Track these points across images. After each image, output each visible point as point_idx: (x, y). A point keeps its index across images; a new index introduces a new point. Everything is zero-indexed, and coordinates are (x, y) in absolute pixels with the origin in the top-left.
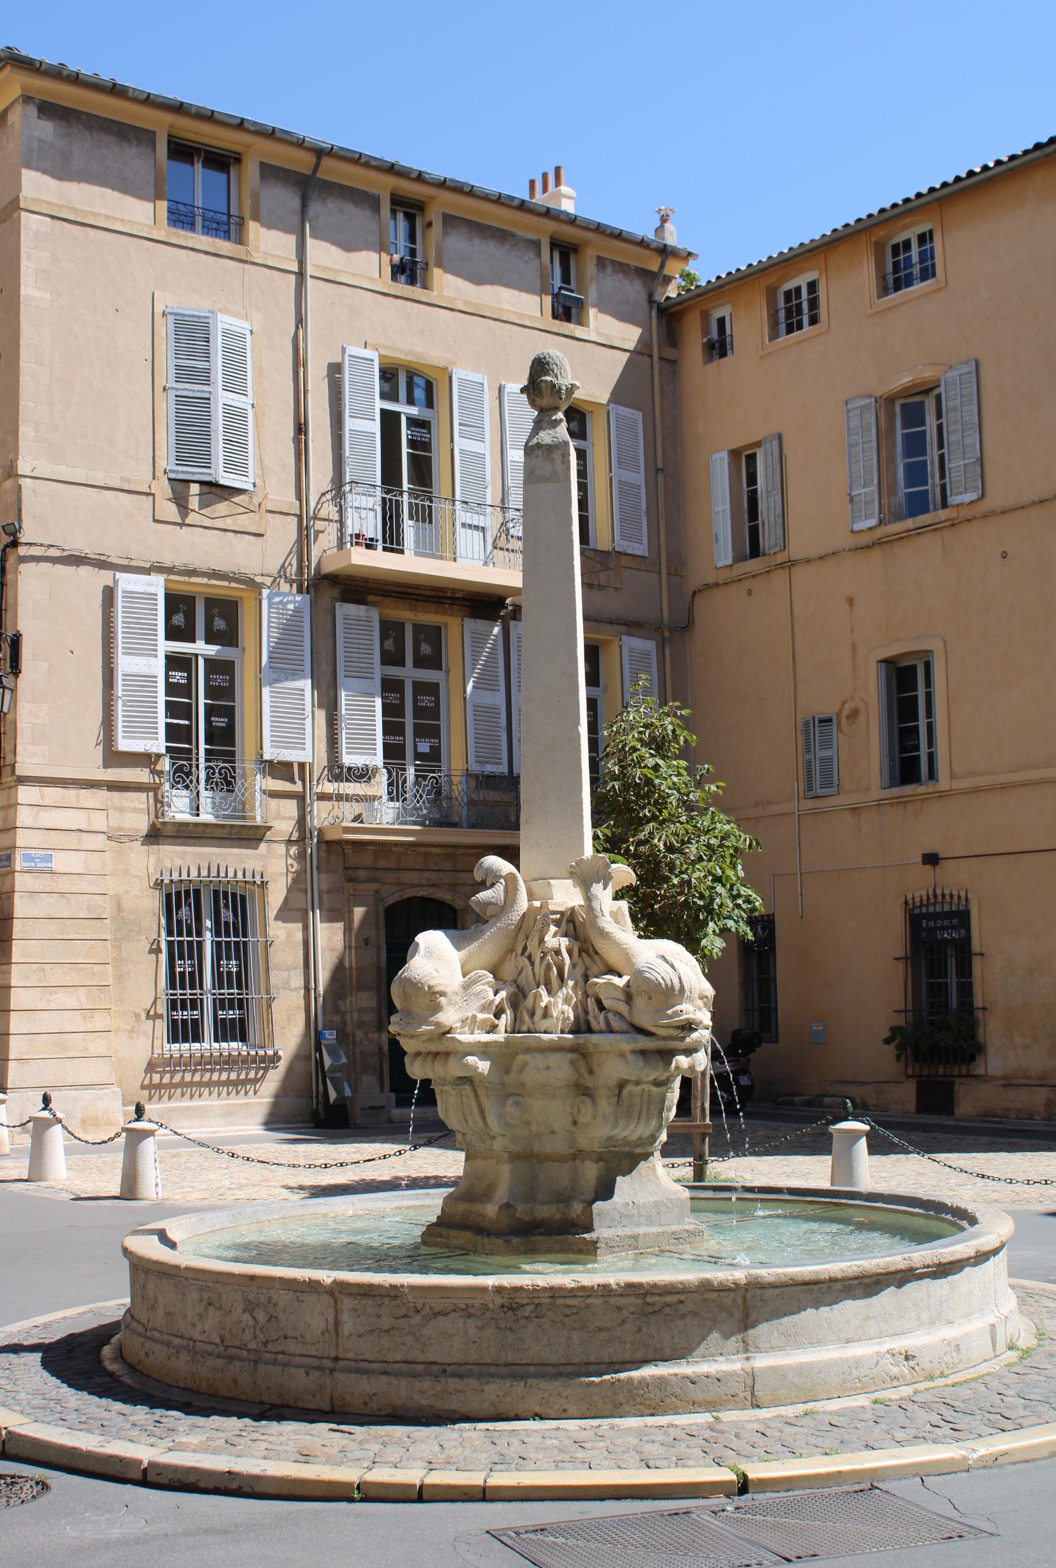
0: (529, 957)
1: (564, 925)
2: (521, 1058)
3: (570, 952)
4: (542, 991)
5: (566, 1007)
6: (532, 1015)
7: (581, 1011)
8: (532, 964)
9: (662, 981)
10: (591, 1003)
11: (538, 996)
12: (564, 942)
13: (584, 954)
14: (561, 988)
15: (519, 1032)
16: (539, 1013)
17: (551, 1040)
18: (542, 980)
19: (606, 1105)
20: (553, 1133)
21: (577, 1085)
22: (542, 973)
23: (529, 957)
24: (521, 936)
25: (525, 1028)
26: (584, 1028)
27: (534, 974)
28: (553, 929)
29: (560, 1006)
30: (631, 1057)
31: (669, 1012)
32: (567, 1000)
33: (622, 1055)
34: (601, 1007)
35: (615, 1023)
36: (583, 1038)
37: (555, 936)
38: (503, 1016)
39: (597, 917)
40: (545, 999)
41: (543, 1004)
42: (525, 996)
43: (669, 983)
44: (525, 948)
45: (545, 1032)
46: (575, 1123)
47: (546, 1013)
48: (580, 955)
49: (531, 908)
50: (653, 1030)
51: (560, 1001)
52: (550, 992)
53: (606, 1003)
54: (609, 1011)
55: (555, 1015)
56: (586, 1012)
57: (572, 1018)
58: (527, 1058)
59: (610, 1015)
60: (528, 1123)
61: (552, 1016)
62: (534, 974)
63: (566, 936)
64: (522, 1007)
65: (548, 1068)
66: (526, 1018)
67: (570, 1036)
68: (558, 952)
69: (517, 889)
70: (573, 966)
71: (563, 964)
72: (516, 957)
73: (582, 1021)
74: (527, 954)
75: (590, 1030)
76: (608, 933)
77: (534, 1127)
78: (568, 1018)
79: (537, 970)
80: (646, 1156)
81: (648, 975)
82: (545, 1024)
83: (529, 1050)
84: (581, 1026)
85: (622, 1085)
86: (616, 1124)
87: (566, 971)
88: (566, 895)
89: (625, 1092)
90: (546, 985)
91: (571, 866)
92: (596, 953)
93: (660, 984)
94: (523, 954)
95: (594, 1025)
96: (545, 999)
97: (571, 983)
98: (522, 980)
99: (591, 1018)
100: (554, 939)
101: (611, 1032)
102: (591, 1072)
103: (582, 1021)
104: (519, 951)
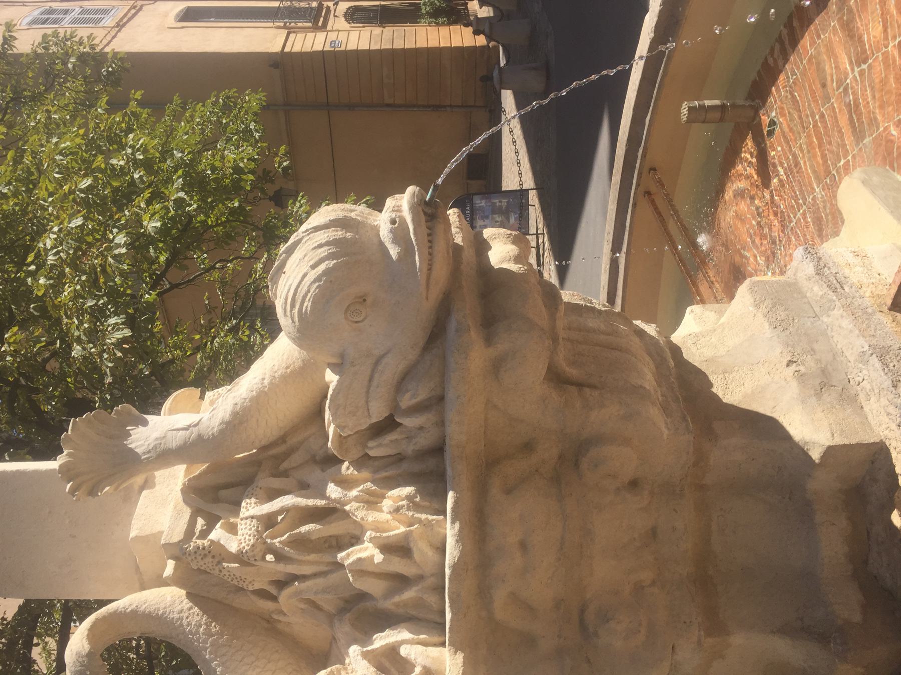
0: (282, 584)
1: (216, 509)
2: (501, 609)
3: (272, 495)
4: (349, 556)
5: (387, 504)
6: (401, 581)
7: (391, 470)
8: (295, 578)
9: (322, 267)
10: (378, 449)
11: (362, 569)
12: (251, 508)
13: (285, 465)
14: (346, 515)
15: (443, 613)
16: (399, 566)
17: (461, 538)
18: (327, 558)
19: (605, 415)
20: (653, 533)
21: (556, 480)
22: (312, 557)
23: (282, 584)
24: (239, 601)
25: (431, 599)
26: (431, 463)
27: (315, 575)
28: (218, 533)
29: (382, 516)
30: (502, 346)
31: (394, 252)
32: (372, 501)
33: (496, 367)
34: (388, 425)
35: (420, 392)
36: (457, 468)
37: (232, 529)
38: (404, 651)
39: (200, 437)
40: (367, 551)
41: (379, 557)
42: (362, 596)
43: (323, 252)
44: (263, 594)
45: (442, 550)
46: (634, 484)
47: (398, 549)
48: (285, 474)
49: (177, 580)
50: (436, 293)
51: (372, 517)
52: (355, 540)
53: (378, 412)
54: (395, 407)
55: (402, 529)
56: (399, 458)
57: (409, 490)
58: (500, 596)
59: (406, 401)
60: (639, 588)
61: (407, 536)
62: (315, 575)
63: (238, 504)
64: (388, 604)
65: (523, 546)
66: (409, 594)
67: (451, 496)
68: (268, 522)
69: (134, 613)
70: (303, 488)
71: (296, 508)
72: (281, 612)
73: (417, 467)
74: (273, 590)
75: (438, 450)
76: (235, 414)
77: (646, 576)
78: (409, 498)
79: (307, 570)
80: (676, 351)
81: (308, 304)
82: (423, 551)
83: (484, 592)
84: (428, 472)
85: (557, 378)
86: (637, 391)
87: (311, 502)
88: (160, 508)
89: (572, 372)
90: (341, 548)
91: (73, 491)
92: (282, 439)
93: (326, 273)
94: (274, 599)
95: (424, 441)
96: (367, 551)
97: (333, 491)
98: (328, 603)
99: (410, 449)
100: (237, 535)
101: (441, 399)
102: (528, 447)
103: (417, 467)
104: (268, 605)
